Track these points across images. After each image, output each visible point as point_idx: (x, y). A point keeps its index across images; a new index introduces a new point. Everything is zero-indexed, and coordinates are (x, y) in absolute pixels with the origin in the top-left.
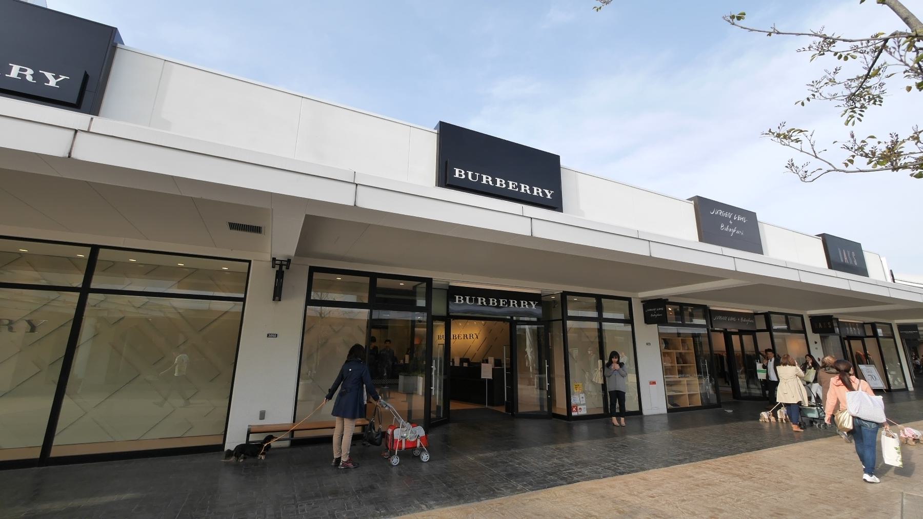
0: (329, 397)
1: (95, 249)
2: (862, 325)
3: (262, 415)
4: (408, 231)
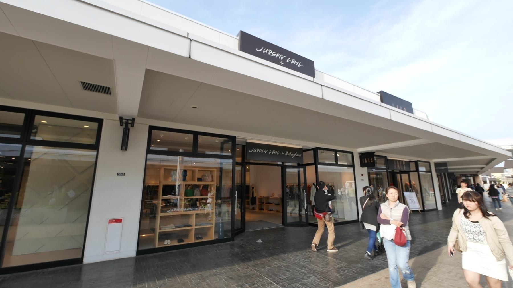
1: (31, 115)
2: (408, 163)
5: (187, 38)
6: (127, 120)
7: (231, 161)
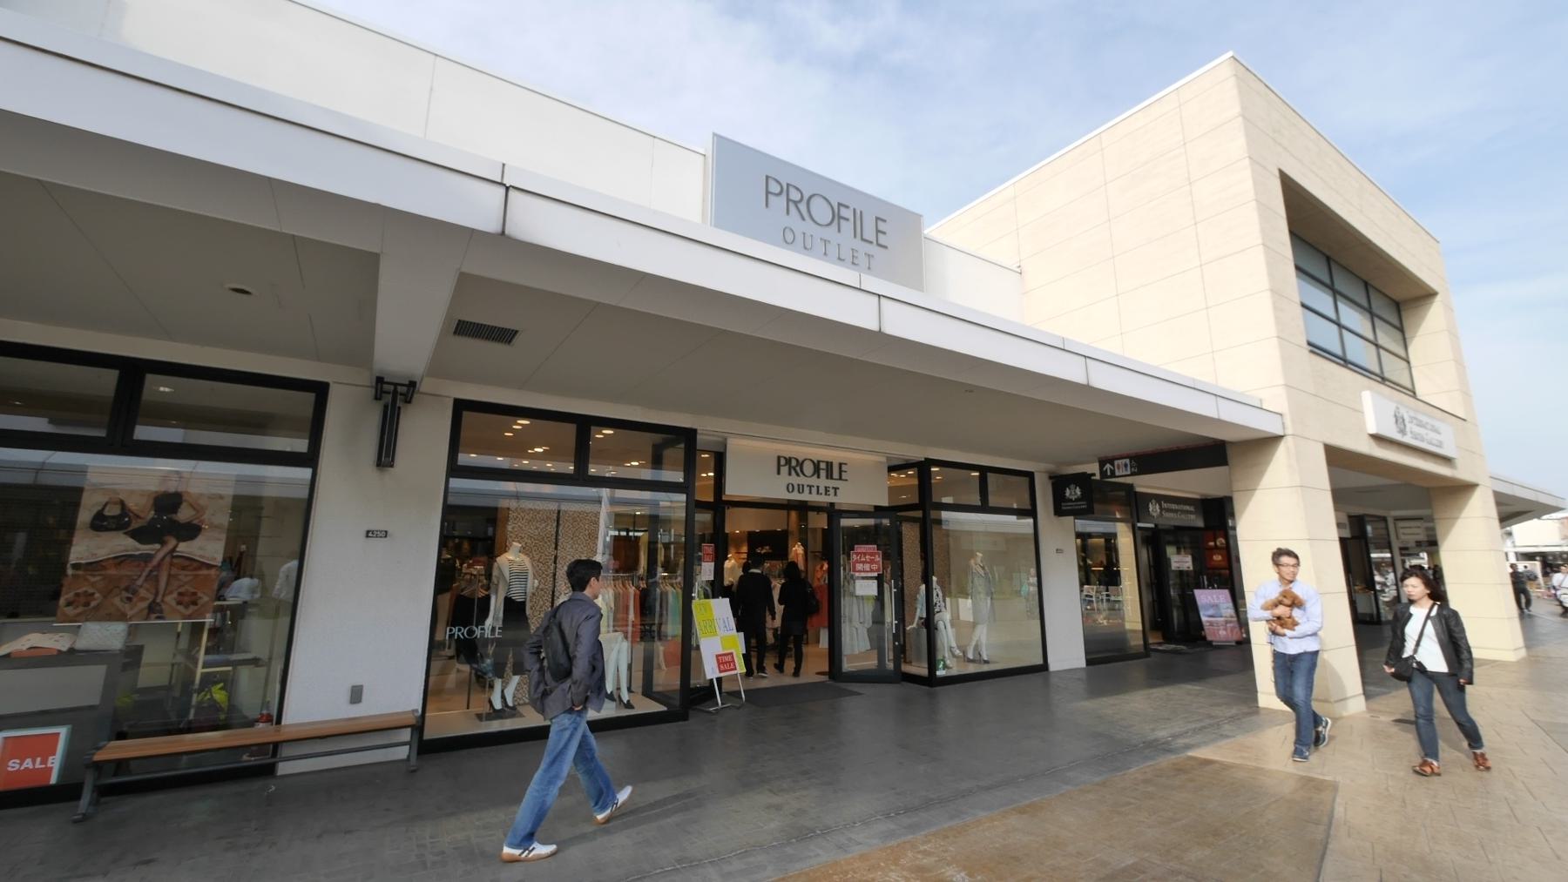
0: (1377, 438)
1: (133, 371)
3: (356, 695)
4: (811, 350)
5: (501, 184)
6: (396, 385)
7: (683, 497)
